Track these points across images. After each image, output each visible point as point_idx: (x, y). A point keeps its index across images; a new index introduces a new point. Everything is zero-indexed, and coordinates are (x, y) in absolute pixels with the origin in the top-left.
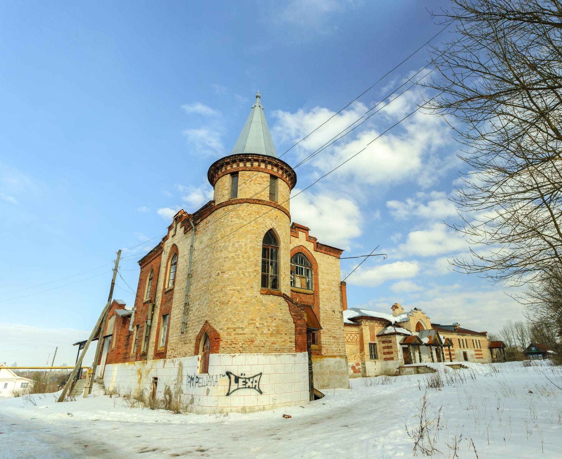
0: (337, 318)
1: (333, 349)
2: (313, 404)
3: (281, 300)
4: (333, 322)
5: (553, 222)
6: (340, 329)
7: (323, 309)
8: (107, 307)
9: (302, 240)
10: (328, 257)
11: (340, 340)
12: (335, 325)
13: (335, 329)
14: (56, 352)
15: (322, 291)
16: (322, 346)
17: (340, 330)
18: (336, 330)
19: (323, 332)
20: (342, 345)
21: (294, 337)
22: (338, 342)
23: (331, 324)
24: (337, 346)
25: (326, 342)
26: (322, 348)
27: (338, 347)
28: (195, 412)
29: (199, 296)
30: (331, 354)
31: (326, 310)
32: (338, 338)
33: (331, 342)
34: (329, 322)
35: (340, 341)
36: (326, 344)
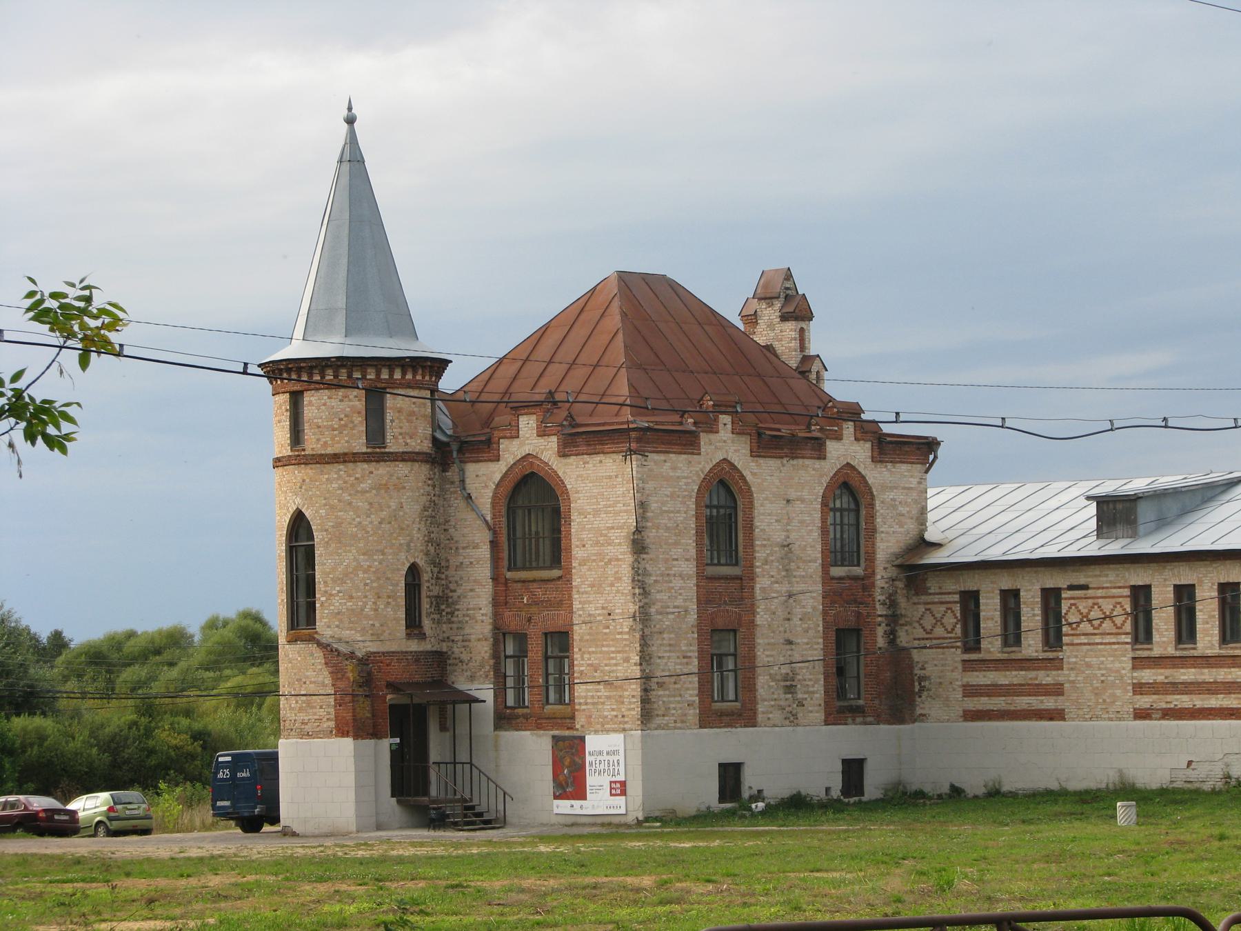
0: (621, 633)
1: (606, 713)
3: (486, 652)
4: (608, 646)
6: (628, 661)
7: (581, 613)
9: (528, 438)
10: (601, 462)
11: (627, 690)
12: (613, 652)
13: (614, 661)
14: (43, 373)
15: (580, 565)
17: (625, 665)
18: (616, 665)
19: (579, 675)
20: (630, 703)
21: (332, 710)
23: (601, 652)
24: (615, 707)
25: (586, 697)
27: (619, 710)
28: (272, 679)
29: (666, 661)
30: (599, 726)
31: (590, 615)
32: (621, 687)
34: (597, 646)
35: (626, 693)
36: (586, 704)
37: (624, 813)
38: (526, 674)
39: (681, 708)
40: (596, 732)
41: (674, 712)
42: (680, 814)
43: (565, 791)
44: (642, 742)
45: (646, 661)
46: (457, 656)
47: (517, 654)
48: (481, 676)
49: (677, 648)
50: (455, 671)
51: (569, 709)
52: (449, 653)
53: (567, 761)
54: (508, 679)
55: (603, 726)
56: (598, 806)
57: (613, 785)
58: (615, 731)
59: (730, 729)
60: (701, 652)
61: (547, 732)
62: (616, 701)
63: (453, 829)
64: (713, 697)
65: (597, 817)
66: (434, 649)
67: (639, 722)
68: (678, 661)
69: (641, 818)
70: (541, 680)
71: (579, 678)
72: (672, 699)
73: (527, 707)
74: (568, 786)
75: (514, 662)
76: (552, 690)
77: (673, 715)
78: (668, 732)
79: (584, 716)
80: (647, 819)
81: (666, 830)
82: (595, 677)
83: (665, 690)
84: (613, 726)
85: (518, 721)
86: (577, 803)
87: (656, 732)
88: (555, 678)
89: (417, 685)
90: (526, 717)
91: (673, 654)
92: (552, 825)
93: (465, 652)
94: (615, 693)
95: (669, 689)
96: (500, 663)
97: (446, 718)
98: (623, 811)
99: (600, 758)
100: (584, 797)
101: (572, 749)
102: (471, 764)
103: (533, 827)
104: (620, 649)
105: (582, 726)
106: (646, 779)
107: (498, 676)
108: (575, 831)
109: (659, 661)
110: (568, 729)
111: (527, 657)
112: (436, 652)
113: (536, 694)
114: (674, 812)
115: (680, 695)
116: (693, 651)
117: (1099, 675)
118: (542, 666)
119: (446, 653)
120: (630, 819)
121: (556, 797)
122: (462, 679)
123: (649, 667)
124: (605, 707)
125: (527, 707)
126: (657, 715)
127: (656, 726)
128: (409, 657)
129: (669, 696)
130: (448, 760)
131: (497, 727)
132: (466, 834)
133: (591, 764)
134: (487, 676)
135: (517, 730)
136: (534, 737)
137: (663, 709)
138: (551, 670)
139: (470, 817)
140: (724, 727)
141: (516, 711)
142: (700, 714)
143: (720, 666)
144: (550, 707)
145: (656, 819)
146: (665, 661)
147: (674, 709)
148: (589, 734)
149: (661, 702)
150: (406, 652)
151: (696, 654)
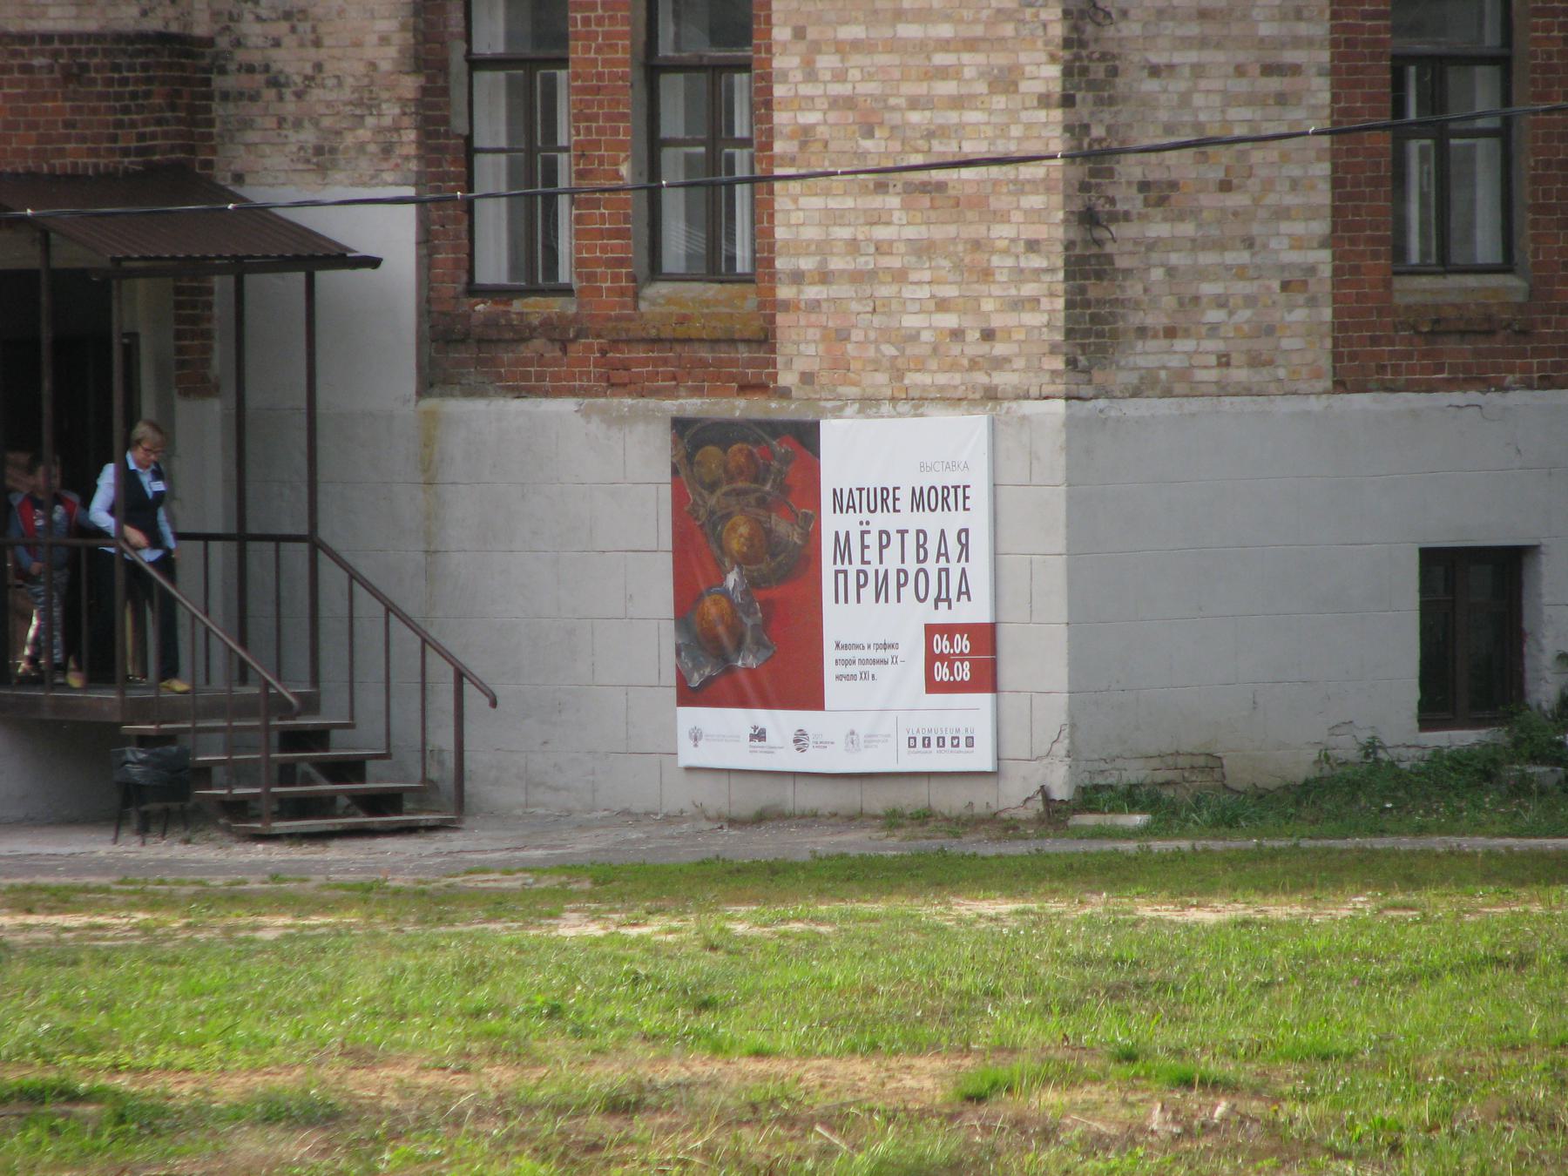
1: (910, 321)
2: (1419, 753)
3: (384, 40)
5: (737, 77)
8: (1259, 856)
11: (1003, 217)
12: (945, 45)
13: (947, 88)
16: (784, 292)
17: (1000, 101)
18: (958, 102)
20: (1019, 275)
22: (976, 245)
23: (893, 45)
24: (950, 291)
25: (823, 248)
26: (781, 319)
27: (971, 305)
29: (1183, 86)
30: (882, 378)
32: (978, 203)
33: (881, 248)
36: (825, 277)
37: (987, 765)
38: (562, 140)
39: (1250, 301)
40: (868, 404)
41: (1214, 315)
42: (1239, 774)
43: (730, 670)
44: (1068, 448)
45: (1092, 85)
46: (256, 58)
47: (527, 51)
48: (361, 147)
49: (1236, 29)
50: (247, 124)
51: (749, 300)
52: (223, 42)
53: (739, 535)
54: (480, 161)
55: (898, 375)
56: (871, 738)
57: (942, 645)
58: (950, 400)
59: (1473, 396)
60: (1345, 45)
61: (652, 402)
62: (958, 267)
63: (228, 830)
64: (1400, 252)
65: (867, 785)
66: (153, 24)
67: (1059, 363)
68: (1241, 86)
69: (1061, 792)
70: (624, 170)
71: (792, 161)
72: (1207, 258)
73: (566, 291)
74: (739, 645)
75: (510, 82)
76: (674, 205)
77: (1214, 329)
78: (1193, 405)
79: (813, 333)
80: (1089, 797)
81: (1158, 845)
82: (864, 155)
83: (1181, 217)
84: (942, 379)
85: (527, 351)
86: (781, 722)
87: (1134, 408)
88: (689, 159)
89: (72, 183)
90: (560, 334)
91: (1220, 57)
92: (668, 819)
93: (289, 41)
94: (951, 230)
95: (1194, 213)
96: (445, 91)
97: (207, 335)
98: (981, 759)
99: (881, 520)
100: (809, 696)
101: (758, 479)
102: (315, 544)
103: (581, 827)
104: (979, 31)
105: (807, 378)
106: (1082, 623)
107: (442, 149)
108: (765, 845)
109: (1151, 85)
110: (745, 388)
111: (563, 62)
112: (163, 38)
113: (601, 234)
114: (1212, 763)
115: (1249, 243)
116: (1310, 42)
117: (1020, 363)
118: (631, 101)
119: (209, 42)
120: (1014, 795)
121: (688, 696)
122: (276, 160)
123: (1107, 115)
124: (908, 292)
125: (566, 291)
126: (1142, 332)
127: (1133, 378)
128: (38, 61)
129: (1196, 245)
130: (215, 527)
131: (432, 380)
132: (278, 854)
133: (843, 549)
134: (387, 150)
135: (520, 392)
136: (596, 426)
137: (1169, 302)
138: (673, 123)
139: (308, 781)
140: (1449, 385)
141: (517, 305)
142: (1339, 326)
143: (1434, 99)
144: (663, 288)
145: (1130, 798)
146: (1180, 85)
147: (1221, 302)
148: (837, 413)
149: (1157, 274)
150: (25, 38)
151: (1325, 56)
